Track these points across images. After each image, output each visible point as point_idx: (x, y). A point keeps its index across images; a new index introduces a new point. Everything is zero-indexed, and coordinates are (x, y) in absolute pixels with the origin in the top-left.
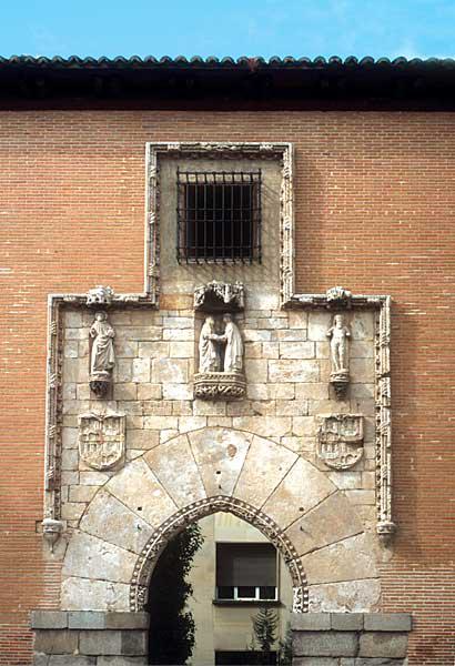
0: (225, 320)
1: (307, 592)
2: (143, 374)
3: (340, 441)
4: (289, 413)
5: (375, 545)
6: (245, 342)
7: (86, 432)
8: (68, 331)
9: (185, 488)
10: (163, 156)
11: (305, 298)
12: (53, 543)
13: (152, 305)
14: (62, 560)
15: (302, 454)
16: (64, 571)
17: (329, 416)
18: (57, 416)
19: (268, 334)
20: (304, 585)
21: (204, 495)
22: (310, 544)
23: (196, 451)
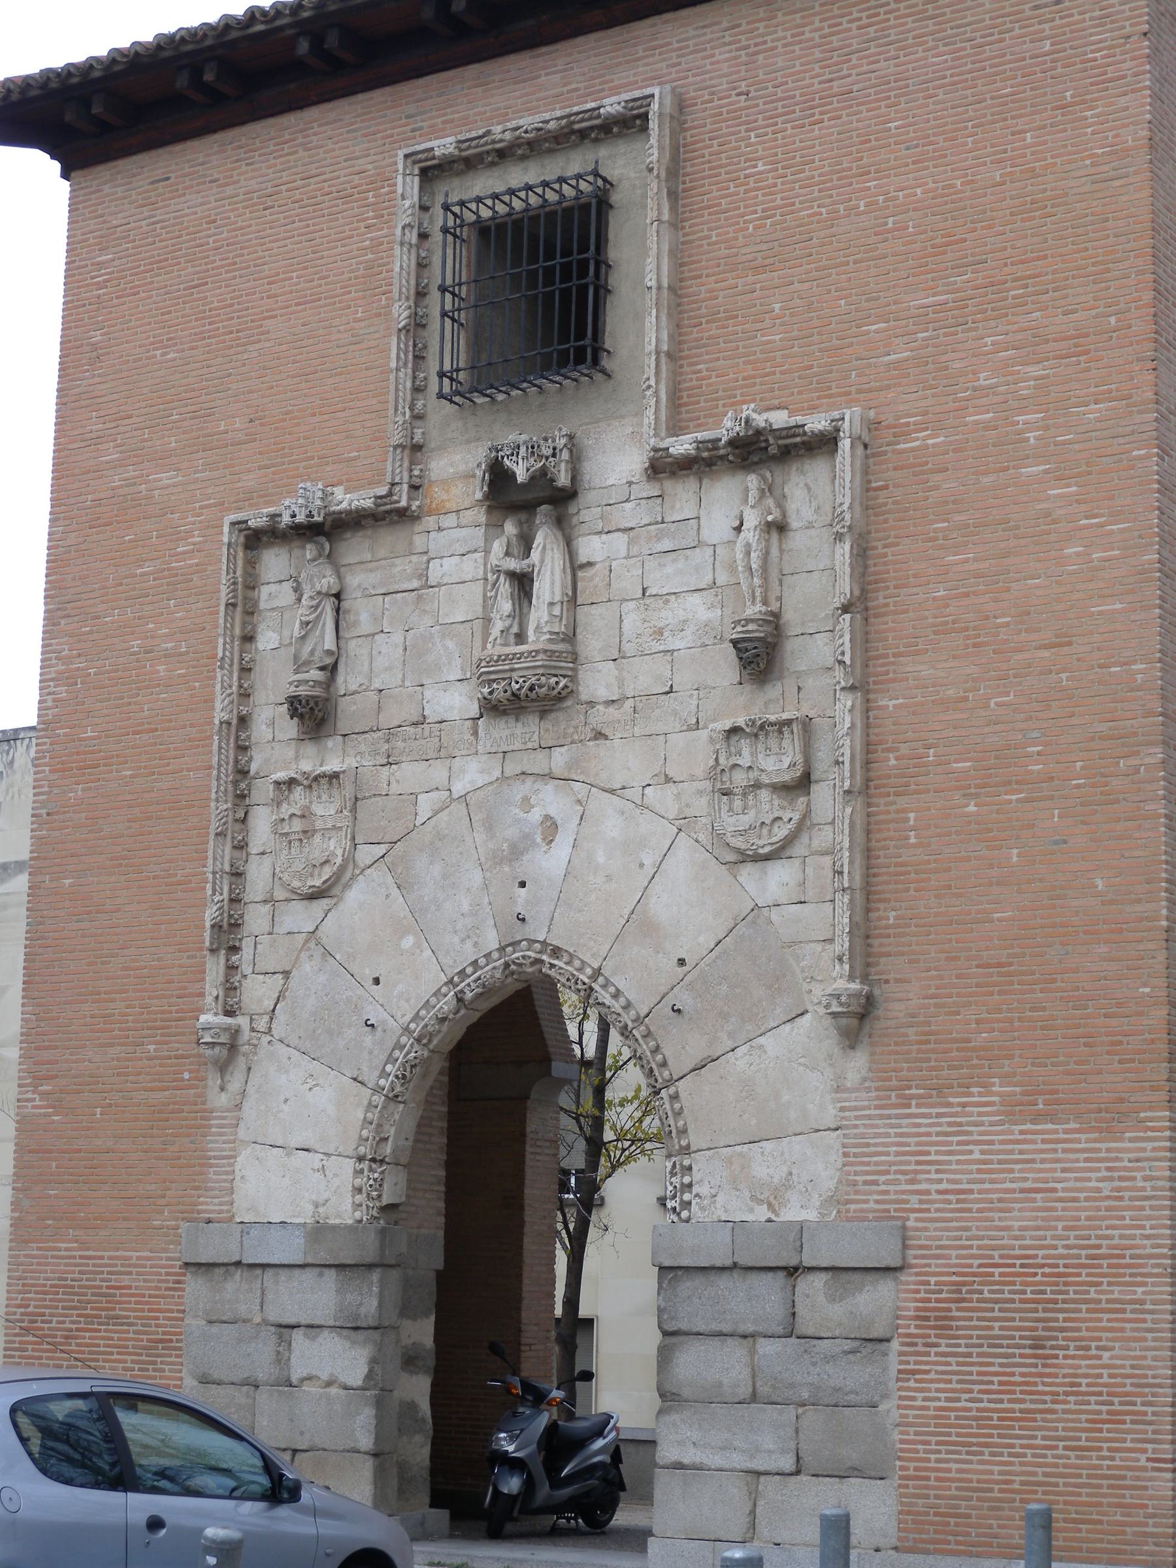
1: (690, 1168)
2: (389, 669)
3: (757, 786)
4: (660, 728)
5: (831, 1042)
6: (575, 567)
7: (286, 810)
8: (265, 591)
9: (459, 926)
11: (682, 446)
12: (223, 1067)
13: (406, 509)
14: (239, 1107)
16: (242, 1133)
18: (236, 783)
19: (620, 540)
20: (686, 1150)
21: (491, 941)
22: (695, 1050)
23: (480, 836)
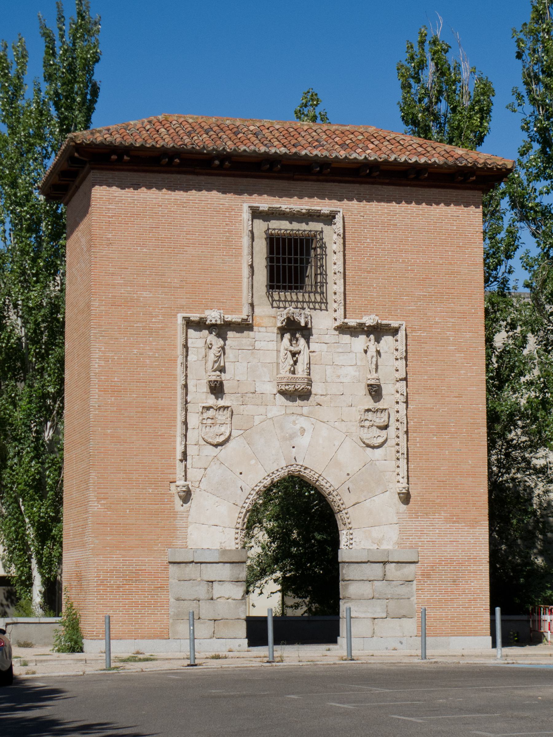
0: (298, 335)
1: (352, 534)
7: (205, 416)
10: (256, 214)
11: (352, 322)
15: (348, 434)
16: (190, 519)
17: (366, 408)
21: (284, 465)
